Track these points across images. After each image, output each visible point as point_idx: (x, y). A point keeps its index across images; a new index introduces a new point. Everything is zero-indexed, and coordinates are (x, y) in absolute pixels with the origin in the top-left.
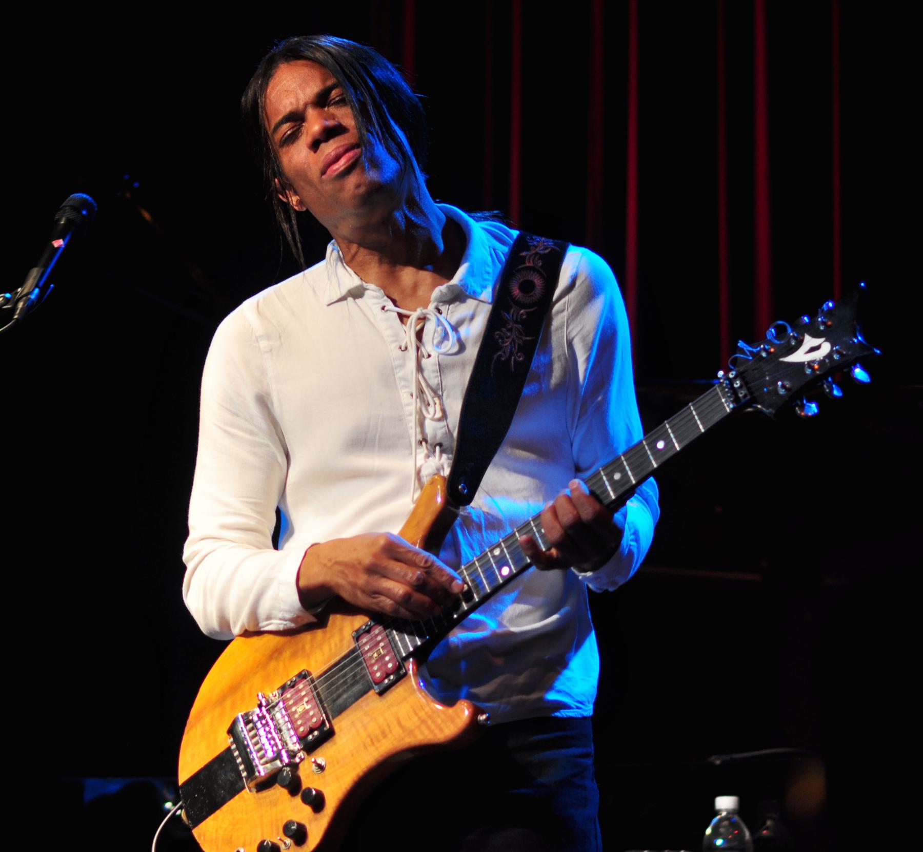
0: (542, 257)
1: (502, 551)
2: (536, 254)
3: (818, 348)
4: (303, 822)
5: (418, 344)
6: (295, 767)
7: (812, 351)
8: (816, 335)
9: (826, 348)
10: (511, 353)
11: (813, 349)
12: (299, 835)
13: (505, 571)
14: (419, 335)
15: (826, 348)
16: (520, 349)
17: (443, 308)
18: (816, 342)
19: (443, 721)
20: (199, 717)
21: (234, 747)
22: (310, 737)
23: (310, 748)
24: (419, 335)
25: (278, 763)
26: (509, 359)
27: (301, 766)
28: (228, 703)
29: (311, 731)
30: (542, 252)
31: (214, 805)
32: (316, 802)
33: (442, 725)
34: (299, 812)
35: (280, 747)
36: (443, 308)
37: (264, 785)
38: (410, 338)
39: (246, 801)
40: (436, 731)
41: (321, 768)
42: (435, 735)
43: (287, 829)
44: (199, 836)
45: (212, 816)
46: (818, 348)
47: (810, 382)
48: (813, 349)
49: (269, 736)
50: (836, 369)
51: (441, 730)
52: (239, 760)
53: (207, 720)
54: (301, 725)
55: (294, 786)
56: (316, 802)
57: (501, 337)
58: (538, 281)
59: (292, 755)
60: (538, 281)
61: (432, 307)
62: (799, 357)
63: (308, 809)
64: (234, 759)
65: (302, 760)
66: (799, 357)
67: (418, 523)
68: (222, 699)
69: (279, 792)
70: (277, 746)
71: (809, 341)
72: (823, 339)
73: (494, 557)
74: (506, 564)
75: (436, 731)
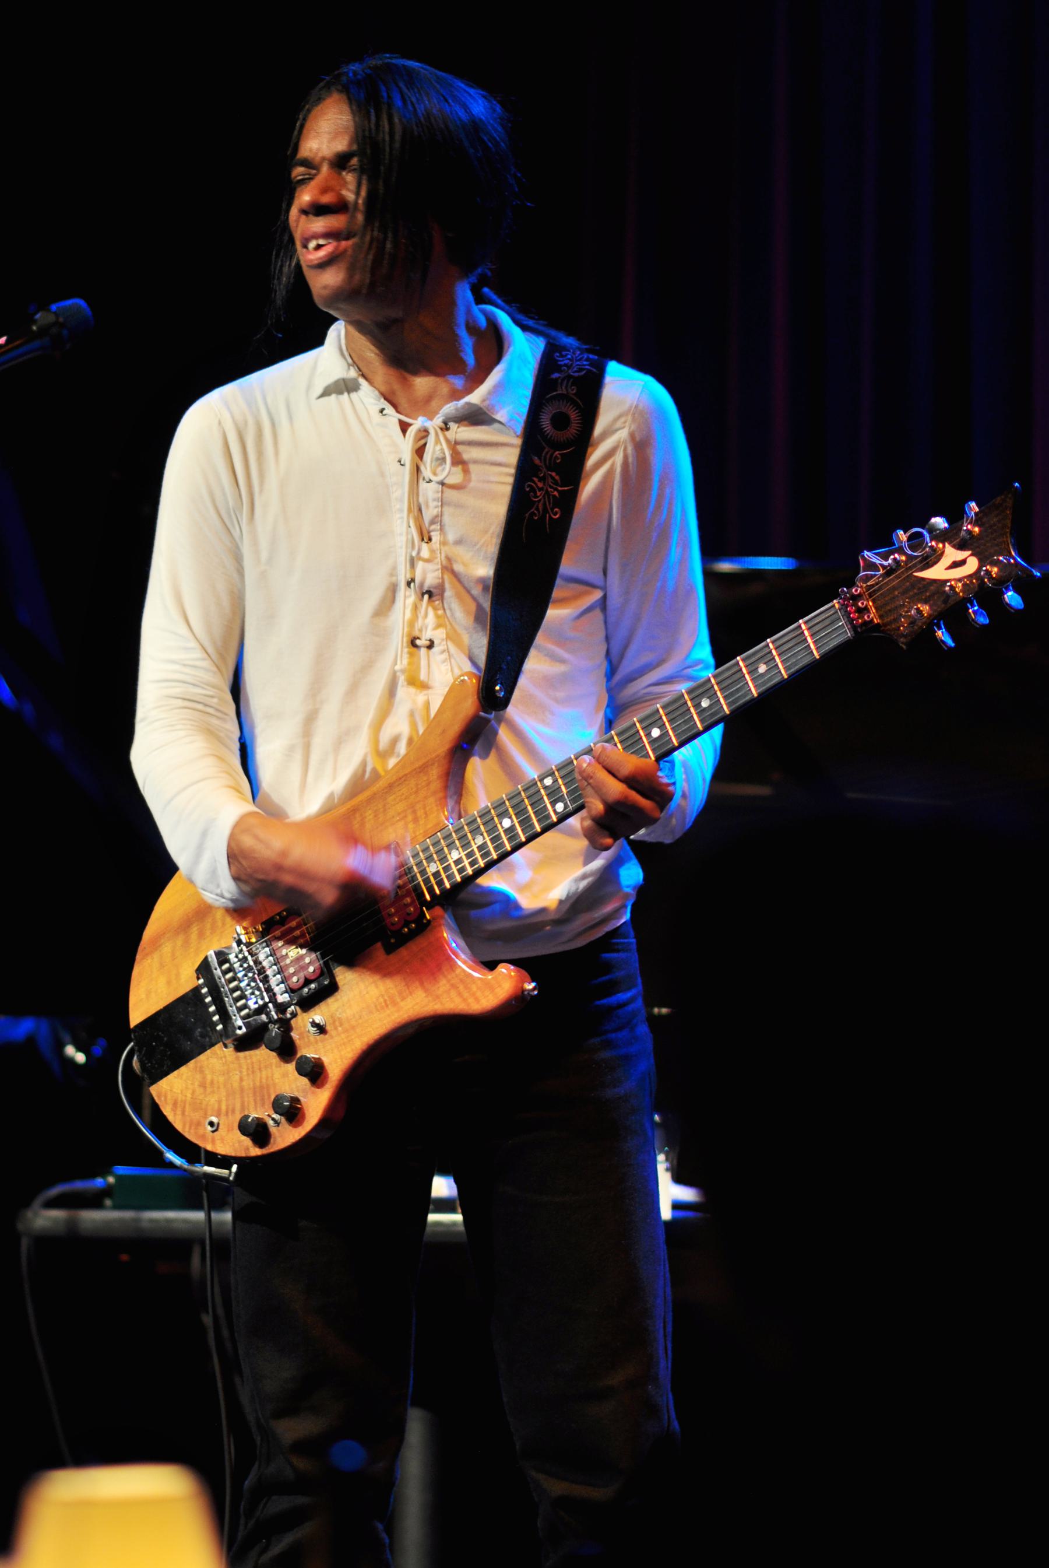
0: (576, 381)
1: (555, 781)
2: (569, 377)
3: (963, 563)
4: (296, 1094)
5: (417, 459)
6: (286, 1025)
7: (952, 567)
8: (961, 547)
9: (972, 564)
10: (545, 510)
11: (956, 565)
12: (292, 1112)
13: (560, 807)
14: (420, 452)
15: (972, 564)
16: (557, 503)
17: (452, 425)
18: (961, 555)
19: (478, 988)
20: (156, 943)
21: (205, 990)
22: (306, 990)
23: (308, 1003)
24: (420, 452)
25: (264, 1017)
26: (543, 517)
27: (293, 1022)
28: (194, 930)
29: (307, 982)
30: (576, 374)
31: (178, 1060)
32: (314, 1072)
33: (479, 994)
34: (288, 1080)
35: (267, 1000)
36: (452, 425)
37: (244, 1044)
38: (407, 456)
39: (218, 1059)
40: (471, 1000)
41: (321, 1029)
42: (468, 1005)
43: (277, 1105)
44: (159, 1097)
45: (176, 1073)
46: (963, 563)
47: (951, 608)
48: (956, 565)
49: (253, 984)
50: (985, 592)
51: (477, 1000)
52: (208, 999)
53: (167, 949)
54: (294, 974)
55: (286, 1050)
56: (314, 1072)
57: (533, 490)
58: (573, 415)
59: (281, 1008)
60: (573, 415)
61: (438, 421)
62: (936, 572)
63: (304, 1081)
64: (202, 997)
65: (294, 1015)
66: (936, 572)
67: (444, 731)
68: (185, 926)
69: (263, 1055)
70: (263, 998)
71: (952, 554)
72: (969, 553)
73: (545, 788)
74: (561, 799)
75: (471, 1000)
